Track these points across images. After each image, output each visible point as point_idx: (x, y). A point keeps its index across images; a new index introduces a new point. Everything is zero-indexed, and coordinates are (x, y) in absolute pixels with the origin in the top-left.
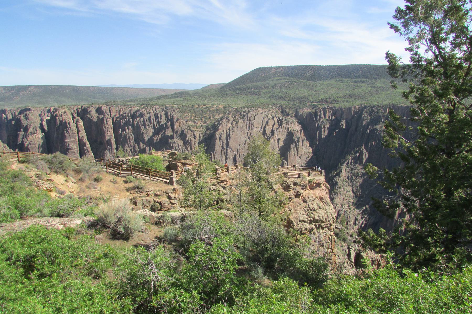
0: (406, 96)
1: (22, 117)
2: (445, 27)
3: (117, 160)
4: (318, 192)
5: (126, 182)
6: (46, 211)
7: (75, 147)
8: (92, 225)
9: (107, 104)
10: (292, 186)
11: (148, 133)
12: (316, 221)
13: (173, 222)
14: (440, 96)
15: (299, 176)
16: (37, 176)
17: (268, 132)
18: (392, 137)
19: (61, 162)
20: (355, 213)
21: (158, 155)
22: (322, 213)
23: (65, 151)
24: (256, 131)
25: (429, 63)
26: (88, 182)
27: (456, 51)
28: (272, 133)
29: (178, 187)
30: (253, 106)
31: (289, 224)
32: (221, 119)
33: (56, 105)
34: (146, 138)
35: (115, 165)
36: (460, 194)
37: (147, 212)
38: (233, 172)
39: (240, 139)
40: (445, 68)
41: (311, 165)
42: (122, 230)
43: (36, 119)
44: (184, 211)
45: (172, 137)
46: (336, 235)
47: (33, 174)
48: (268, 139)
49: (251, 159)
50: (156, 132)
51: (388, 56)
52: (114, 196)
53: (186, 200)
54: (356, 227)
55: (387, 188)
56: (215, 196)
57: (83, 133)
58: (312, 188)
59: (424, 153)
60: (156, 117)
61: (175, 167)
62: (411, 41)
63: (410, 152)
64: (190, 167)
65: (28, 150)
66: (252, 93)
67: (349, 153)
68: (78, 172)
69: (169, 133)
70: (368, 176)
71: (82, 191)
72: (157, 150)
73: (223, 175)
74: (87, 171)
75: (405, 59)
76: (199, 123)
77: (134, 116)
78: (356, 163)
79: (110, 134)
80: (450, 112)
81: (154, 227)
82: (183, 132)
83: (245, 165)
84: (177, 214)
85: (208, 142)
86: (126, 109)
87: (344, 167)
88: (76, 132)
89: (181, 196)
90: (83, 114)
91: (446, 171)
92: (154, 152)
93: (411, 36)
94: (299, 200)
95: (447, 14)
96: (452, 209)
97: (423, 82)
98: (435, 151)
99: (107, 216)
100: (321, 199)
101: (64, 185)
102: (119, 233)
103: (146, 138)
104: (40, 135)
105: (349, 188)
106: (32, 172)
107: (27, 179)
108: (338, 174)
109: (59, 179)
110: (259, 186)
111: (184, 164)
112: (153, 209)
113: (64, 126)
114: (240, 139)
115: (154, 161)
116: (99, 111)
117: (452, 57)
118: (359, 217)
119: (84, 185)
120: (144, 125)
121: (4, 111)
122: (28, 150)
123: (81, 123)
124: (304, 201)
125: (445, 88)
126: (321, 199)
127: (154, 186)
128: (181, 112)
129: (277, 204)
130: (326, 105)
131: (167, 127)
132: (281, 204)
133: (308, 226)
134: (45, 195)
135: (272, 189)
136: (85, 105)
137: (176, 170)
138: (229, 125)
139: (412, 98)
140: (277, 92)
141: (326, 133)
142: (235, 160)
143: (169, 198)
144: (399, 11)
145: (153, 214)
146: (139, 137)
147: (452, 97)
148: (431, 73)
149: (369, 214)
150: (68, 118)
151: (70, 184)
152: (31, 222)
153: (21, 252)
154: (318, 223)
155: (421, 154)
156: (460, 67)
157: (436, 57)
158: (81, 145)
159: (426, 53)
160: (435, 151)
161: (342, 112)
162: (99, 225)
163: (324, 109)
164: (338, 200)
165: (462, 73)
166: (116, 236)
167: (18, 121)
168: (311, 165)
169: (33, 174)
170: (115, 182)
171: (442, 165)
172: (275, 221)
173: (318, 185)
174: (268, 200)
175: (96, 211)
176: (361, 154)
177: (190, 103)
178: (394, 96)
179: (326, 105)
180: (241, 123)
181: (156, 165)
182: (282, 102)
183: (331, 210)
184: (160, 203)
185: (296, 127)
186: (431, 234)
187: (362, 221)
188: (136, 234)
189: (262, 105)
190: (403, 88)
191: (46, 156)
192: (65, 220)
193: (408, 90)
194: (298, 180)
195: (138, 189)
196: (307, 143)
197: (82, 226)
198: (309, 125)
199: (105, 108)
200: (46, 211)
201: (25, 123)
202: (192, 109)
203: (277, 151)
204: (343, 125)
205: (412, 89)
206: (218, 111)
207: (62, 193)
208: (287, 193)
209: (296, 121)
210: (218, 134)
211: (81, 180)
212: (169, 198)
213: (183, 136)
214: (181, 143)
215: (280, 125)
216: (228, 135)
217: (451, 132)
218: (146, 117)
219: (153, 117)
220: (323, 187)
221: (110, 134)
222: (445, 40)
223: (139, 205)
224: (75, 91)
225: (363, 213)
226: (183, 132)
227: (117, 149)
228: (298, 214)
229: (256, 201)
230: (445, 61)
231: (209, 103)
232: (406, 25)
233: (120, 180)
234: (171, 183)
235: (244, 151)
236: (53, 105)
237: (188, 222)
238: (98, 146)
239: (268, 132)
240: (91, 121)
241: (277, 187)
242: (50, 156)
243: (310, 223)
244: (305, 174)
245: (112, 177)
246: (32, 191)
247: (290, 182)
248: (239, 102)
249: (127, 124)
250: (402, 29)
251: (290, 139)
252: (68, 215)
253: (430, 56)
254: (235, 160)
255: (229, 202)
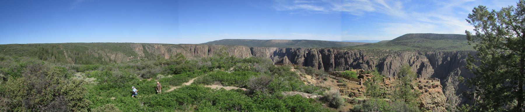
0: (475, 48)
1: (297, 51)
2: (488, 23)
3: (335, 72)
4: (437, 89)
5: (338, 82)
6: (303, 90)
7: (317, 65)
8: (321, 99)
9: (332, 48)
10: (424, 87)
11: (351, 61)
12: (436, 103)
13: (359, 102)
14: (488, 48)
15: (427, 82)
16: (300, 75)
17: (412, 62)
18: (470, 65)
19: (311, 70)
20: (455, 98)
21: (354, 71)
22: (439, 99)
23: (313, 66)
24: (405, 62)
25: (483, 36)
26: (321, 80)
27: (493, 32)
28: (414, 62)
29: (364, 86)
30: (403, 51)
31: (422, 105)
32: (387, 56)
33: (311, 47)
34: (350, 63)
35: (333, 74)
36: (498, 86)
37: (347, 97)
38: (392, 80)
39: (397, 65)
40: (489, 37)
41: (433, 77)
42: (335, 104)
43: (303, 52)
44: (365, 98)
45: (362, 63)
46: (446, 109)
47: (299, 74)
48: (411, 66)
49: (402, 74)
50: (355, 61)
51: (466, 32)
52: (332, 87)
53: (367, 92)
54: (456, 104)
55: (469, 86)
56: (382, 91)
57: (321, 59)
58: (434, 88)
59: (483, 71)
60: (355, 54)
61: (363, 77)
62: (476, 27)
63: (477, 70)
64: (370, 77)
65: (298, 64)
66: (404, 45)
67: (452, 71)
68: (317, 75)
69: (361, 61)
70: (461, 82)
71: (317, 83)
72: (354, 69)
73: (387, 81)
74: (321, 76)
75: (474, 33)
76: (376, 57)
77: (345, 54)
78: (455, 75)
79: (332, 61)
80: (493, 55)
81: (349, 104)
82: (368, 61)
83: (399, 77)
84: (361, 99)
85: (380, 67)
86: (342, 51)
87: (450, 78)
88: (319, 58)
89: (365, 91)
90: (322, 52)
91: (492, 78)
92: (353, 70)
93: (476, 25)
94: (427, 94)
95: (488, 18)
96: (496, 92)
97: (481, 43)
98: (487, 70)
99: (328, 96)
100: (439, 92)
101: (310, 80)
102: (333, 104)
103: (350, 63)
104: (303, 59)
105: (453, 87)
106: (298, 73)
107: (296, 75)
108: (447, 81)
109: (309, 77)
110: (406, 87)
111: (367, 76)
112: (350, 96)
113: (313, 56)
114: (397, 65)
115: (352, 74)
116: (329, 51)
117: (491, 34)
118: (458, 99)
119: (319, 81)
120: (349, 58)
121: (291, 49)
122: (298, 64)
123: (320, 55)
124: (430, 94)
125: (490, 45)
126: (439, 92)
127: (351, 85)
128: (367, 52)
129: (415, 95)
130: (440, 51)
131: (360, 59)
132: (417, 96)
133: (432, 106)
134: (302, 83)
135: (413, 88)
136: (323, 48)
137: (363, 78)
138: (391, 59)
139: (477, 49)
140: (416, 44)
141: (441, 63)
142: (394, 75)
143: (359, 91)
144: (470, 15)
145: (349, 98)
146: (346, 62)
147: (493, 49)
148: (484, 40)
149: (462, 98)
150: (316, 53)
151: (313, 80)
152: (296, 93)
153: (292, 104)
154: (437, 104)
155: (482, 71)
156: (495, 38)
157: (486, 33)
158: (319, 64)
159: (481, 32)
160: (487, 70)
161: (448, 54)
162: (324, 99)
163: (440, 52)
164: (447, 92)
165: (496, 40)
166: (331, 105)
167: (295, 52)
168: (433, 77)
169: (299, 74)
170: (333, 82)
171: (490, 75)
172: (413, 104)
173: (437, 86)
174: (410, 94)
175: (324, 93)
176: (458, 71)
177: (372, 49)
178: (471, 48)
179: (440, 51)
180: (397, 58)
181: (353, 75)
182: (419, 49)
183: (444, 98)
184: (354, 93)
185: (426, 60)
186: (488, 104)
187: (459, 101)
188: (341, 106)
189: (409, 50)
190: (473, 45)
191: (305, 67)
192: (310, 95)
193: (475, 46)
194: (427, 84)
195: (344, 85)
196: (431, 67)
197: (317, 98)
198: (432, 59)
199: (331, 50)
200: (303, 90)
201: (298, 53)
202: (373, 51)
203: (416, 71)
204: (449, 59)
205: (477, 45)
206: (386, 52)
207: (309, 83)
208: (421, 91)
209: (426, 58)
210: (385, 62)
211: (318, 79)
212: (359, 91)
213: (368, 63)
214: (367, 66)
215: (418, 59)
216: (391, 63)
217: (493, 62)
218: (350, 54)
219: (353, 54)
220: (439, 87)
221: (332, 61)
222: (489, 28)
223: (344, 93)
224: (320, 43)
225: (459, 97)
226: (368, 61)
227: (335, 67)
228: (426, 100)
229: (403, 95)
230: (489, 36)
231: (381, 49)
232: (473, 21)
233: (335, 81)
234: (360, 84)
235: (398, 71)
236: (310, 47)
237: (367, 103)
238: (327, 64)
239: (412, 62)
240: (325, 55)
241: (416, 87)
242: (306, 67)
243: (433, 104)
244: (430, 81)
245: (332, 79)
246: (298, 80)
247: (422, 85)
248: (397, 49)
249: (342, 57)
250: (472, 22)
251: (423, 65)
252: (311, 93)
253: (483, 33)
254: (394, 75)
255: (389, 94)
